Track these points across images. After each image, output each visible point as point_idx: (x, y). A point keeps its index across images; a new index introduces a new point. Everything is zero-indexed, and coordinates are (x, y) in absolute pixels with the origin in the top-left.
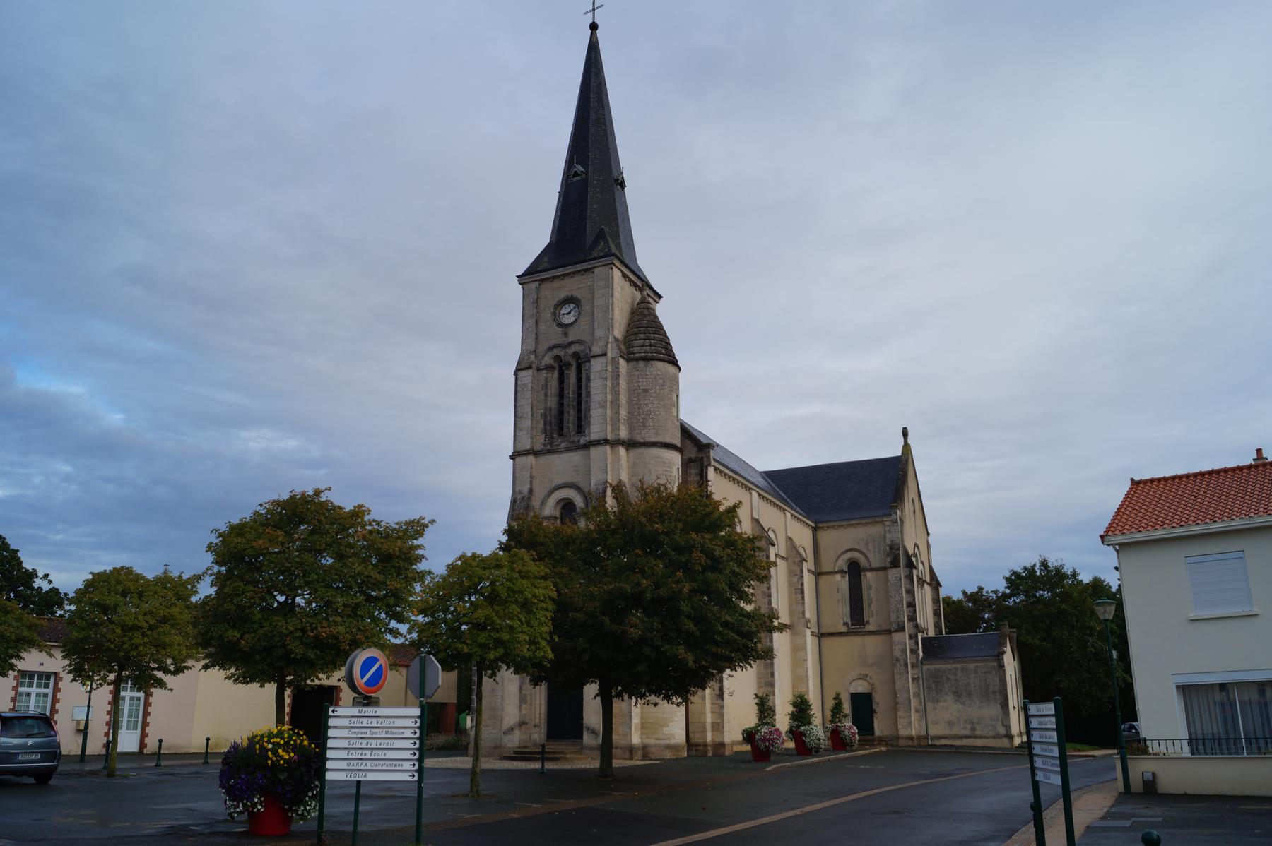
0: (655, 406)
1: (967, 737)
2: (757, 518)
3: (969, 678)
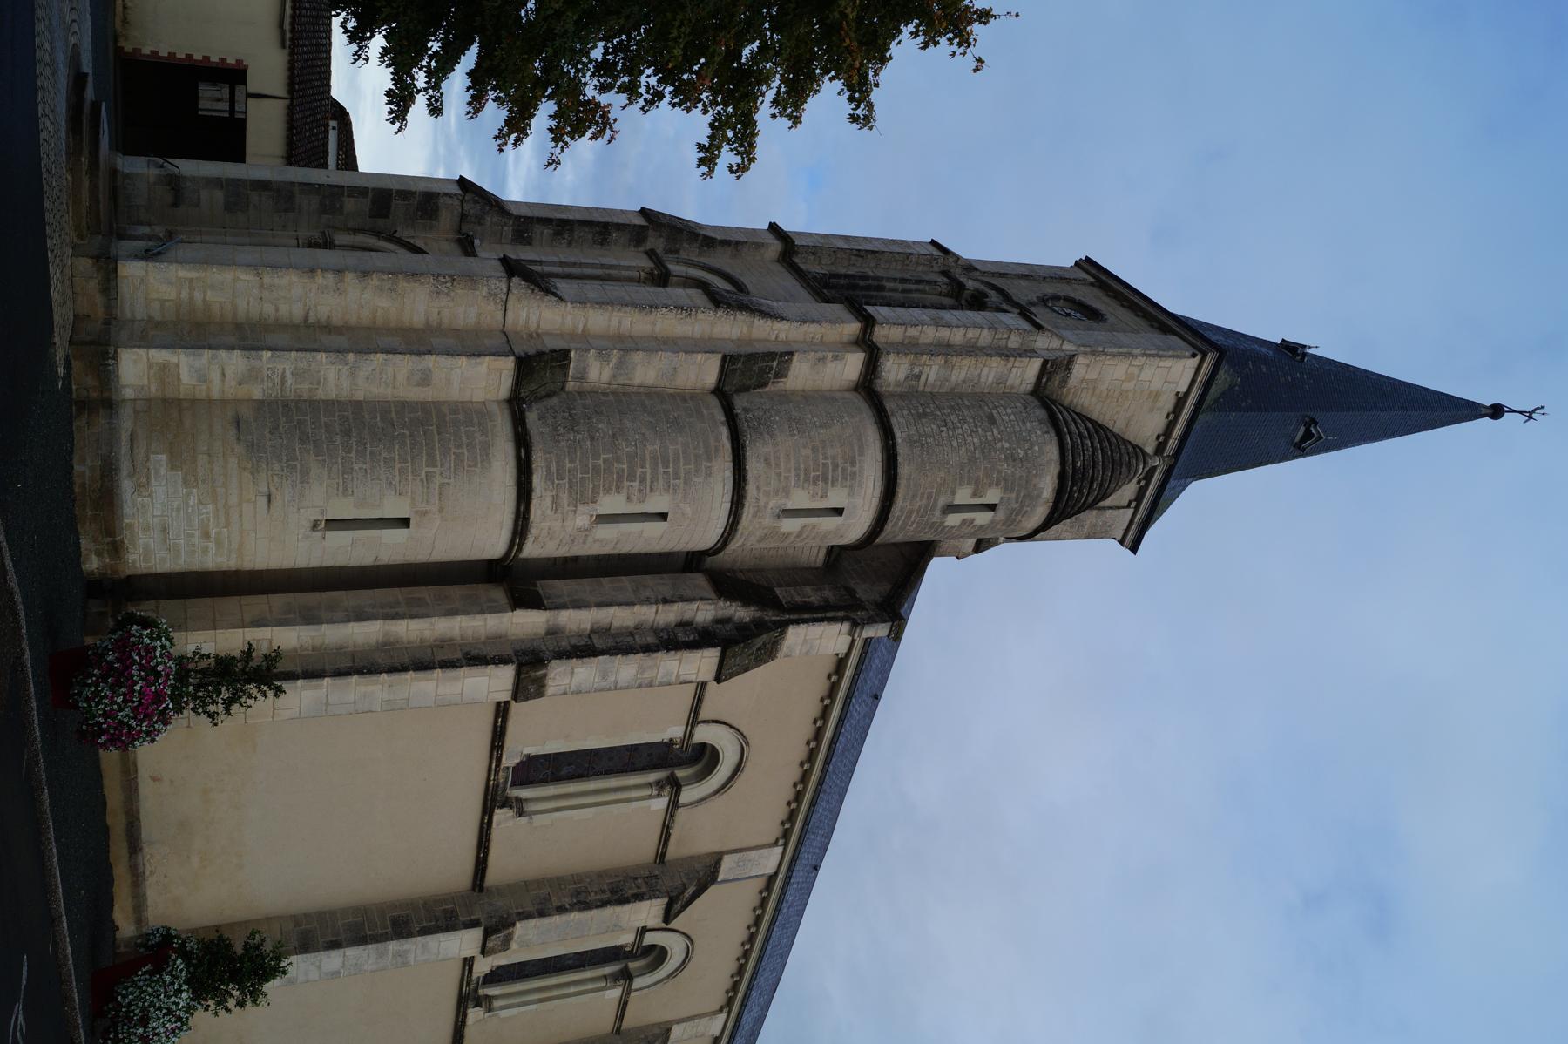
2: (720, 878)
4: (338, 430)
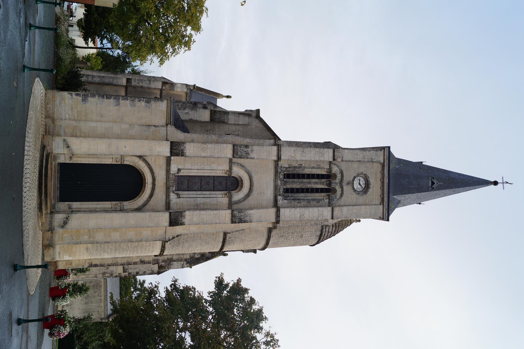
4: (113, 249)
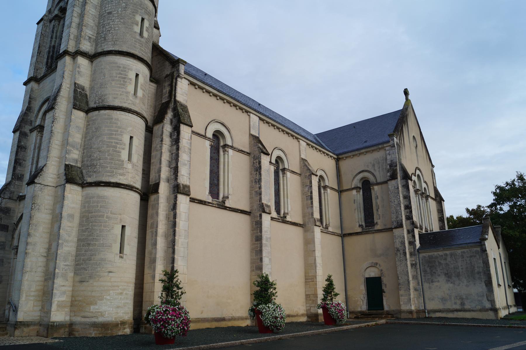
0: (116, 23)
1: (457, 310)
3: (457, 262)
4: (88, 248)
